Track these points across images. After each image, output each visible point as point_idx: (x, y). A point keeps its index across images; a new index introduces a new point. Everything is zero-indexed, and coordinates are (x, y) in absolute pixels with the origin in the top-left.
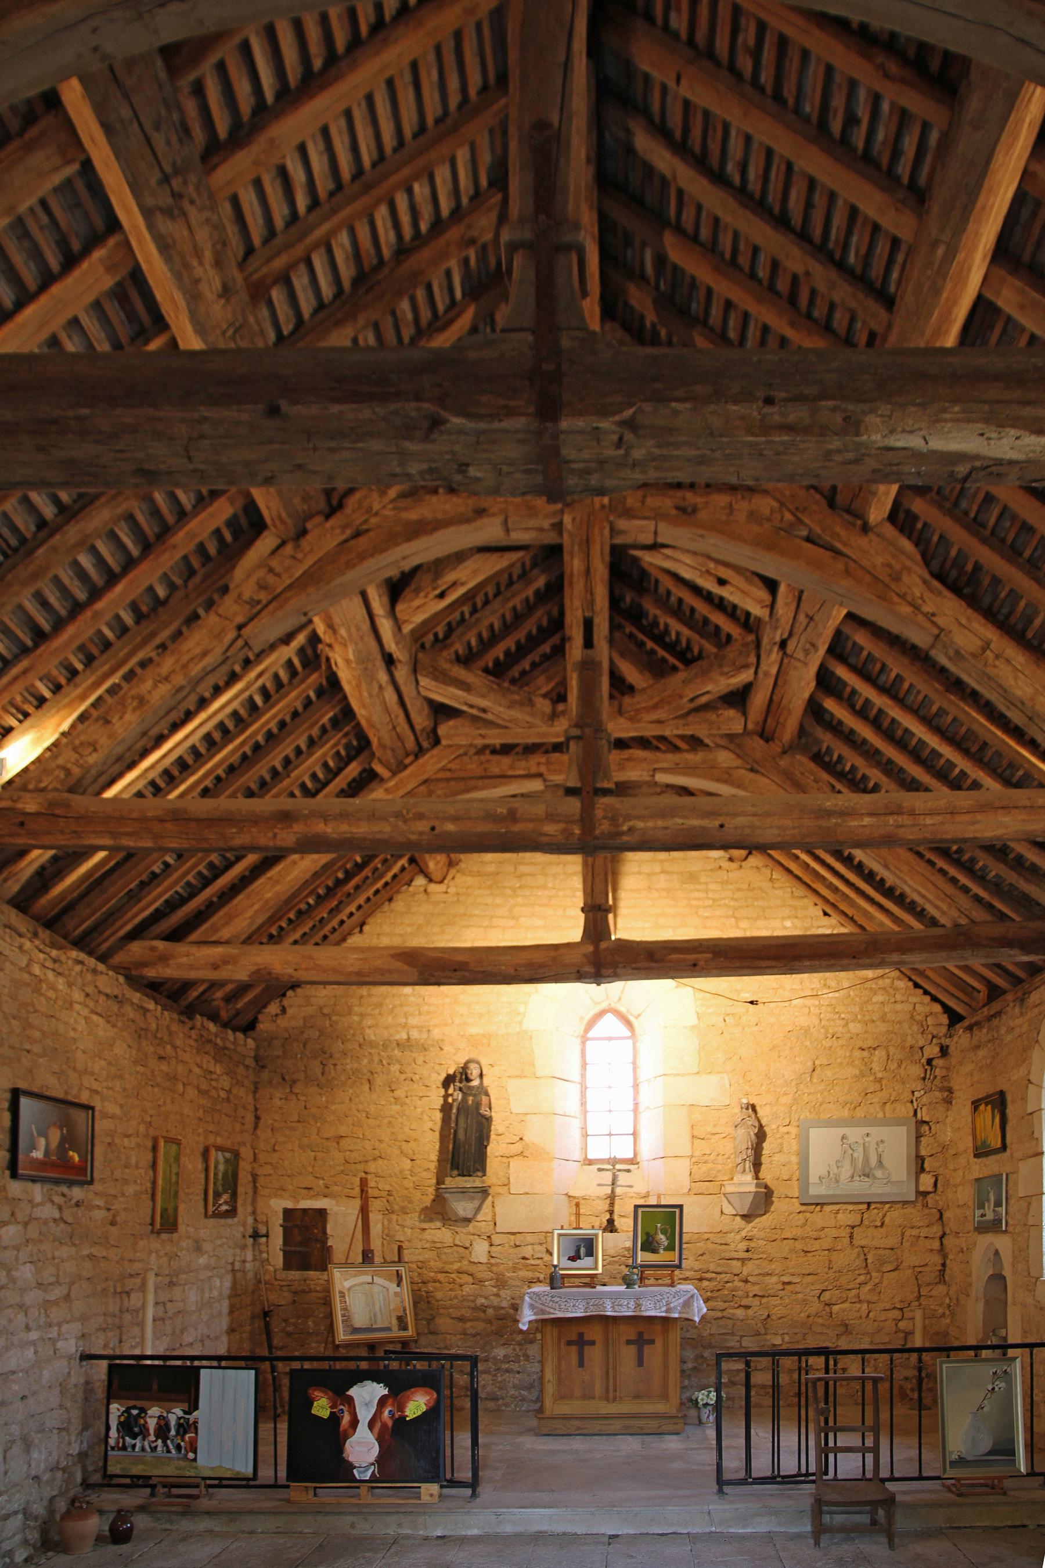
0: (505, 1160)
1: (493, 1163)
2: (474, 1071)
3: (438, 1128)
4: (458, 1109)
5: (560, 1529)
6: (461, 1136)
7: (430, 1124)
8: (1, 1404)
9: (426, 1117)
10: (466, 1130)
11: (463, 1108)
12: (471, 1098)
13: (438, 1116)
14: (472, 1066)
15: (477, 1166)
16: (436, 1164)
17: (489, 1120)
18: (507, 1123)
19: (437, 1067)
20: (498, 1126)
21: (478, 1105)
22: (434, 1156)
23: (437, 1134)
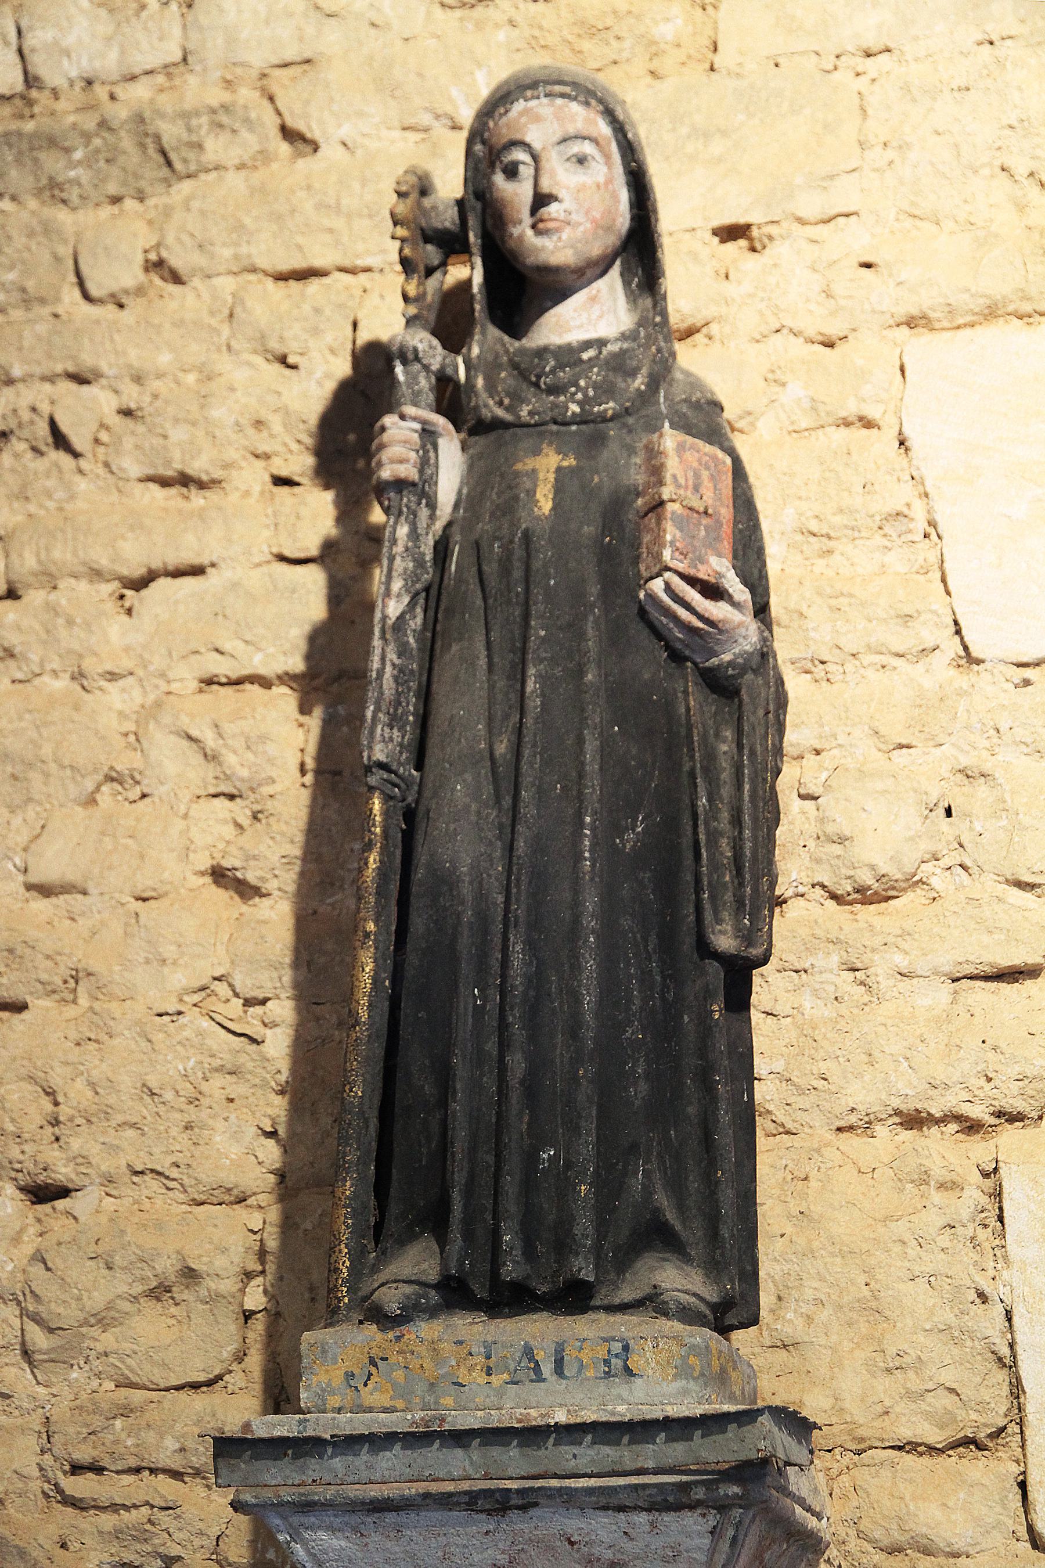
0: (940, 1148)
1: (821, 1199)
2: (575, 210)
3: (276, 852)
4: (433, 596)
5: (698, 1411)
6: (463, 843)
7: (214, 830)
8: (320, 1564)
9: (171, 764)
10: (506, 781)
11: (482, 581)
12: (546, 465)
13: (283, 739)
14: (539, 123)
15: (647, 1184)
16: (263, 1217)
17: (743, 695)
18: (930, 770)
19: (268, 301)
20: (843, 787)
21: (622, 525)
22: (242, 1144)
23: (276, 917)
